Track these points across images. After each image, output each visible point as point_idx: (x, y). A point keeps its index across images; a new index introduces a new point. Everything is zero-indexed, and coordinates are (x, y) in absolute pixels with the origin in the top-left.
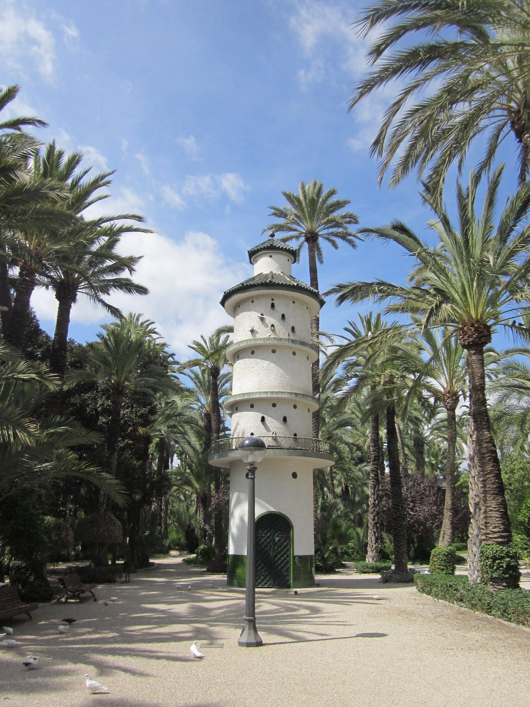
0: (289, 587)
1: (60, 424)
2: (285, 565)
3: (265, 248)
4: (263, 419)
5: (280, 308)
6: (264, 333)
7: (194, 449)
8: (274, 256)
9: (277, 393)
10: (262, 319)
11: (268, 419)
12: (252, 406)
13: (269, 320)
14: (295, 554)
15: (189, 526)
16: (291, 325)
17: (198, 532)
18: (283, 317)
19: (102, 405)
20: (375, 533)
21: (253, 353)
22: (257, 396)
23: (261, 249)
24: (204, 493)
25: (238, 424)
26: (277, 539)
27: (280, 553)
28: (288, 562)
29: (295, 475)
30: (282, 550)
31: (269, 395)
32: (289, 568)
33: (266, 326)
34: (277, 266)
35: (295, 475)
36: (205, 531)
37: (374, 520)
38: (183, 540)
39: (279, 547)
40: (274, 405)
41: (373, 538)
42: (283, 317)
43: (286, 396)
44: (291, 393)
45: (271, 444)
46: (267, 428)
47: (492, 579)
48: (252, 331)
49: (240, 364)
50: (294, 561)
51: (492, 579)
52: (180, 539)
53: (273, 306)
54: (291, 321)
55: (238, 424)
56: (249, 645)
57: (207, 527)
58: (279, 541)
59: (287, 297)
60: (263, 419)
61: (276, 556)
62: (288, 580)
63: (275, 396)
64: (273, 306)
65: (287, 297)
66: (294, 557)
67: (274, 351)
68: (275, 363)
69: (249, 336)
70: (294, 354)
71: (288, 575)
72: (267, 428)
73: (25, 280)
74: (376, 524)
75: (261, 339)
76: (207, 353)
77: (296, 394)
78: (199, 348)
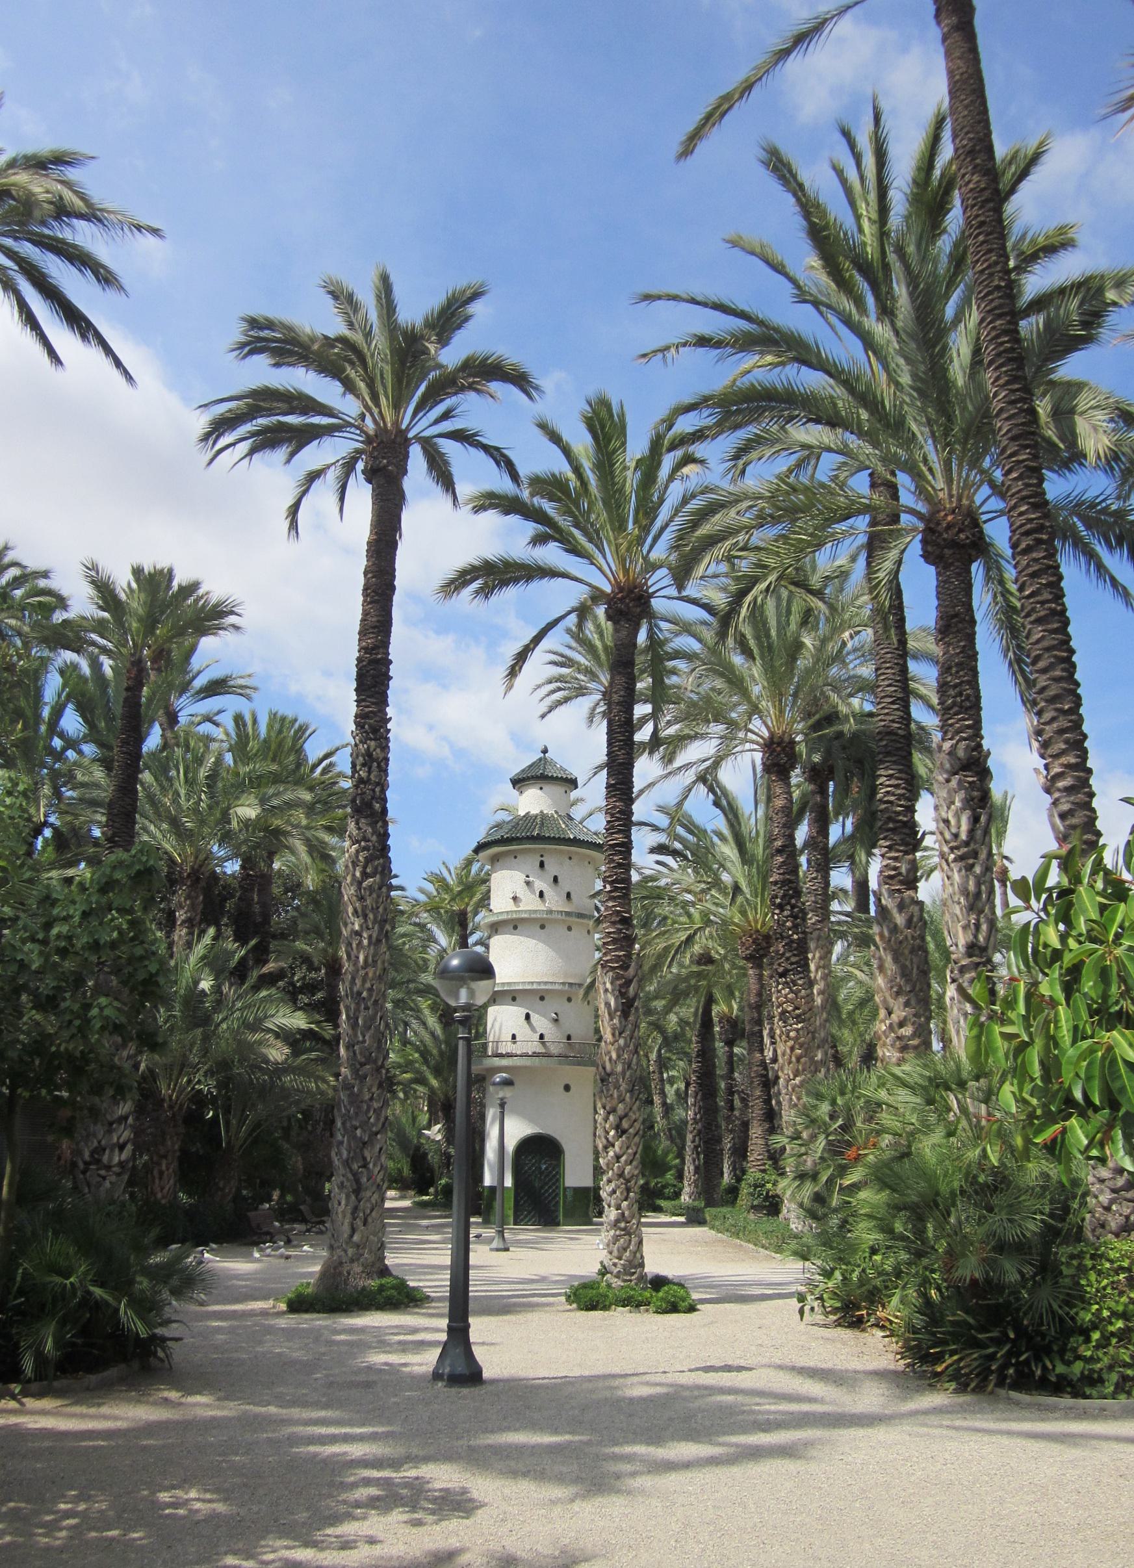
0: (558, 1224)
1: (311, 1050)
2: (554, 1198)
3: (533, 778)
4: (528, 1017)
5: (552, 868)
6: (530, 903)
7: (432, 1034)
8: (547, 788)
9: (546, 983)
10: (528, 883)
11: (535, 1017)
12: (514, 999)
13: (539, 885)
14: (567, 1184)
15: (418, 1148)
16: (567, 890)
17: (433, 1159)
18: (556, 879)
19: (304, 978)
20: (694, 1160)
21: (515, 928)
22: (521, 987)
23: (528, 779)
24: (446, 1096)
25: (495, 1020)
26: (544, 1167)
27: (546, 1184)
28: (557, 1195)
29: (567, 1088)
30: (550, 1180)
31: (535, 987)
32: (558, 1202)
33: (533, 892)
34: (549, 802)
35: (567, 1088)
36: (448, 1156)
37: (693, 1141)
38: (406, 1172)
39: (547, 1176)
40: (542, 998)
41: (692, 1168)
42: (556, 879)
43: (557, 987)
44: (564, 984)
45: (538, 1050)
46: (533, 1029)
47: (753, 1207)
48: (515, 899)
49: (496, 942)
50: (565, 1196)
51: (753, 1207)
52: (400, 1171)
53: (542, 865)
54: (566, 885)
55: (495, 1020)
56: (498, 1250)
57: (452, 1151)
58: (546, 1169)
59: (561, 851)
60: (528, 1017)
61: (542, 1187)
62: (557, 1217)
63: (543, 987)
64: (542, 865)
65: (561, 851)
66: (565, 1189)
67: (543, 927)
68: (544, 942)
69: (511, 906)
70: (569, 929)
71: (557, 1210)
72: (533, 1029)
73: (249, 875)
74: (696, 1147)
75: (526, 911)
76: (452, 890)
77: (571, 984)
78: (439, 881)
